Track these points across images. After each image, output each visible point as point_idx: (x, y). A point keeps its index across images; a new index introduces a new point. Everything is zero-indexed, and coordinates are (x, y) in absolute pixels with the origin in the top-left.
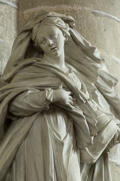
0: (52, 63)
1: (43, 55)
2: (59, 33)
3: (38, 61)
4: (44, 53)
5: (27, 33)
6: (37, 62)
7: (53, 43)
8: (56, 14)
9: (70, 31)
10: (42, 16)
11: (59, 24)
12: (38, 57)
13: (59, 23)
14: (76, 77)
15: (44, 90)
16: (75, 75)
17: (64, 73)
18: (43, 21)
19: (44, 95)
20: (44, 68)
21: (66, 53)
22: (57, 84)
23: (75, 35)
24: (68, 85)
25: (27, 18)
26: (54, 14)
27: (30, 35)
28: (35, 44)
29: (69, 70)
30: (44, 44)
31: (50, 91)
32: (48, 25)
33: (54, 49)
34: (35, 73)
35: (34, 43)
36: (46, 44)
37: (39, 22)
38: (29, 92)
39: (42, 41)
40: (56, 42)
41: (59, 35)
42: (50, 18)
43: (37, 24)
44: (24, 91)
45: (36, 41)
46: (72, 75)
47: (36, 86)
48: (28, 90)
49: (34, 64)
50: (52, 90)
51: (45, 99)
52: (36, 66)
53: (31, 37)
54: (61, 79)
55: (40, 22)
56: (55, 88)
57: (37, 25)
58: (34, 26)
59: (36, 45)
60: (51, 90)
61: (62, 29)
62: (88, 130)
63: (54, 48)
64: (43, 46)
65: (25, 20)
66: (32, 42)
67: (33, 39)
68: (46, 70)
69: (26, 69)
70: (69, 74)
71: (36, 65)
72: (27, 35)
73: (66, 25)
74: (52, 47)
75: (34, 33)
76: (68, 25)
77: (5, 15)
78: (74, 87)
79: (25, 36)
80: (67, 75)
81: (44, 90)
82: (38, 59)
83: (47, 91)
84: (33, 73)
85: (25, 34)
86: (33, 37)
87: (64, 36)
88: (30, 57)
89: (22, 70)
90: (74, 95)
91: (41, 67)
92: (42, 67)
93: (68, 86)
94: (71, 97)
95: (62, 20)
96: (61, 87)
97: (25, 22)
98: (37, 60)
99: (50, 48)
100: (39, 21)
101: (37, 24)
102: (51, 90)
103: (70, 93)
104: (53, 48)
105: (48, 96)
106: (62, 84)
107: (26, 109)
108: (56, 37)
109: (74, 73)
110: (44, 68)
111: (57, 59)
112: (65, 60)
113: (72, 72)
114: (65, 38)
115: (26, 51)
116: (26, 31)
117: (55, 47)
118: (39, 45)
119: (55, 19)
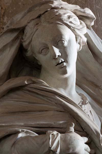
0: (57, 88)
1: (40, 72)
2: (70, 38)
3: (34, 82)
4: (42, 69)
5: (15, 35)
6: (32, 85)
7: (60, 55)
8: (65, 5)
9: (86, 35)
10: (42, 7)
11: (71, 22)
12: (30, 74)
13: (71, 20)
14: (93, 112)
15: (44, 133)
16: (91, 109)
17: (75, 103)
18: (43, 16)
19: (45, 144)
20: (43, 96)
21: (78, 71)
22: (65, 123)
23: (94, 41)
24: (83, 127)
25: (7, 5)
26: (61, 5)
27: (20, 38)
28: (28, 53)
29: (82, 99)
30: (45, 55)
31: (56, 136)
32: (52, 23)
33: (62, 64)
35: (26, 51)
36: (49, 55)
37: (37, 18)
38: (20, 135)
40: (65, 54)
41: (69, 41)
42: (56, 10)
43: (33, 19)
44: (11, 133)
45: (29, 49)
46: (87, 108)
47: (31, 126)
48: (19, 132)
49: (26, 88)
50: (60, 135)
51: (47, 149)
52: (29, 91)
53: (21, 41)
54: (71, 115)
55: (39, 17)
56: (63, 130)
57: (33, 22)
58: (29, 23)
59: (29, 54)
60: (57, 134)
63: (62, 62)
64: (42, 59)
65: (4, 8)
66: (21, 50)
67: (25, 44)
68: (46, 99)
69: (12, 95)
70: (83, 106)
71: (30, 89)
72: (15, 37)
73: (81, 23)
74: (57, 61)
75: (28, 35)
76: (85, 25)
77: (8, 11)
78: (93, 129)
79: (11, 39)
80: (80, 108)
81: (44, 133)
82: (34, 79)
83: (51, 136)
85: (10, 38)
87: (78, 42)
88: (17, 76)
89: (5, 97)
90: (92, 142)
91: (38, 94)
92: (39, 93)
93: (82, 128)
94: (87, 146)
95: (74, 15)
96: (72, 129)
97: (3, 11)
98: (32, 81)
99: (54, 63)
100: (37, 15)
101: (33, 19)
102: (57, 134)
103: (86, 139)
104: (60, 62)
105: (52, 144)
106: (74, 124)
108: (66, 44)
109: (90, 105)
110: (43, 96)
111: (65, 83)
112: (76, 84)
113: (88, 103)
114: (79, 45)
115: (11, 66)
116: (12, 31)
117: (63, 61)
118: (34, 55)
119: (65, 14)
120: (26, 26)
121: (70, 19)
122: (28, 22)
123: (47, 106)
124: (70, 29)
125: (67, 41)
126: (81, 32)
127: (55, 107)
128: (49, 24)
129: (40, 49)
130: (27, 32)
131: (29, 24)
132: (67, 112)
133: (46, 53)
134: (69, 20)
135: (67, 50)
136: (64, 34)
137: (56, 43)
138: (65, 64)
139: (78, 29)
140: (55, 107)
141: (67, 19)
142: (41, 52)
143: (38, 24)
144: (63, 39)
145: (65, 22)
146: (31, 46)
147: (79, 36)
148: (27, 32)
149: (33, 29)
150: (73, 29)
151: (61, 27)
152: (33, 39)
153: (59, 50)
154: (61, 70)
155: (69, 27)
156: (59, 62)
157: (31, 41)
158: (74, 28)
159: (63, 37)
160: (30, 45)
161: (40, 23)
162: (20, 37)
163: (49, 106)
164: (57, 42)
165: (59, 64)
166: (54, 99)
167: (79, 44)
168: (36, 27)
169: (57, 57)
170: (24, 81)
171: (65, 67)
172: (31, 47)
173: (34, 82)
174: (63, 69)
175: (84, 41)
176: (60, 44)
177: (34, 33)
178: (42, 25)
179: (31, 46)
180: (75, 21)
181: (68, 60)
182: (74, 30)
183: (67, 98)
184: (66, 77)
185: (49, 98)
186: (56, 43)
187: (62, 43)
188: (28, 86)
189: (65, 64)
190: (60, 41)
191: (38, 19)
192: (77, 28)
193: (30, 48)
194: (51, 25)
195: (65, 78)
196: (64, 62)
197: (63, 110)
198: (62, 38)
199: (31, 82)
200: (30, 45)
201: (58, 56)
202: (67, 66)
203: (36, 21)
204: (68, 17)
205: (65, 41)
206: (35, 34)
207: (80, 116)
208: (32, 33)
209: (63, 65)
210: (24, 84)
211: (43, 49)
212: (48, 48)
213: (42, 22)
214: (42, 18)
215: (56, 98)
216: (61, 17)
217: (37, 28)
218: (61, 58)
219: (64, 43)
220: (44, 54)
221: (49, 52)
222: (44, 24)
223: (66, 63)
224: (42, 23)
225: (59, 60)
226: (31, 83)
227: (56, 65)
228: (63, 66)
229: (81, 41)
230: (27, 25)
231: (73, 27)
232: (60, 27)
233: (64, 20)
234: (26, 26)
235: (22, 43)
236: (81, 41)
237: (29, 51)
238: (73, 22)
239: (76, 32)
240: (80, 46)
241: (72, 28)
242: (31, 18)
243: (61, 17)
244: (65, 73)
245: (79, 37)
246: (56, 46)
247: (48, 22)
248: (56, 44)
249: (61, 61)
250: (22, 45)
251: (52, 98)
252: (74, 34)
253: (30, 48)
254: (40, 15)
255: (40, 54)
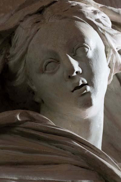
3: (32, 119)
6: (29, 124)
11: (98, 20)
13: (98, 16)
27: (4, 52)
30: (53, 73)
32: (65, 18)
33: (83, 88)
34: (21, 154)
36: (59, 73)
39: (44, 64)
41: (96, 51)
43: (30, 15)
45: (21, 70)
53: (5, 58)
54: (100, 175)
55: (40, 11)
57: (29, 19)
58: (22, 21)
59: (19, 81)
61: (107, 35)
62: (79, 147)
63: (84, 85)
67: (11, 63)
68: (54, 148)
74: (76, 81)
75: (19, 44)
84: (15, 152)
86: (13, 56)
99: (70, 86)
101: (30, 15)
104: (81, 83)
107: (77, 22)
108: (90, 54)
117: (86, 82)
118: (29, 83)
120: (17, 26)
121: (98, 14)
122: (21, 20)
123: (57, 156)
124: (97, 32)
125: (93, 49)
126: (115, 41)
127: (70, 159)
128: (61, 19)
129: (43, 62)
130: (18, 38)
131: (23, 24)
132: (93, 170)
133: (54, 69)
134: (95, 16)
135: (92, 65)
136: (88, 37)
137: (73, 52)
138: (89, 88)
139: (110, 34)
140: (70, 159)
141: (93, 14)
142: (46, 70)
143: (39, 22)
144: (86, 45)
145: (89, 18)
146: (25, 62)
147: (111, 47)
148: (18, 38)
149: (29, 30)
150: (102, 31)
151: (82, 25)
152: (29, 50)
153: (79, 63)
154: (82, 99)
155: (96, 28)
156: (79, 83)
157: (26, 53)
158: (104, 30)
159: (86, 41)
160: (24, 60)
161: (42, 21)
162: (3, 51)
163: (61, 157)
164: (75, 48)
165: (78, 87)
166: (69, 145)
167: (109, 67)
168: (35, 26)
169: (75, 74)
170: (16, 114)
171: (89, 93)
172: (25, 66)
173: (32, 119)
174: (85, 96)
175: (118, 62)
176: (80, 54)
177: (31, 37)
178: (47, 23)
179: (25, 62)
180: (104, 21)
181: (94, 82)
182: (104, 35)
183: (92, 147)
184: (88, 119)
185: (61, 145)
186: (73, 52)
187: (85, 50)
188: (21, 125)
189: (89, 88)
190: (81, 48)
191: (39, 15)
192: (108, 31)
193: (22, 67)
194: (63, 21)
195: (85, 120)
196: (87, 84)
197: (87, 166)
198: (84, 42)
199: (27, 119)
200: (24, 60)
201: (77, 72)
202: (91, 92)
203: (34, 18)
204: (92, 12)
205: (90, 49)
206: (34, 38)
207: (117, 175)
208: (28, 37)
209: (86, 89)
210: (15, 121)
211: (50, 62)
212: (58, 61)
213: (46, 18)
214: (47, 12)
215: (74, 143)
216: (82, 10)
217: (38, 28)
218: (81, 77)
219: (87, 52)
220: (51, 71)
221: (59, 68)
222: (49, 21)
223: (90, 86)
224: (47, 21)
225: (79, 80)
226: (26, 121)
227: (72, 90)
228: (85, 91)
229: (114, 62)
230: (19, 24)
231: (102, 29)
232: (81, 26)
233: (86, 14)
234: (17, 26)
235: (8, 61)
236: (114, 62)
237: (19, 75)
238: (101, 20)
239: (106, 39)
240: (111, 72)
241: (100, 29)
242: (26, 13)
243: (82, 10)
244: (88, 104)
245: (111, 50)
246: (73, 57)
247: (59, 16)
248: (73, 54)
249: (83, 81)
250: (8, 65)
251: (66, 144)
252: (103, 43)
253: (22, 67)
254: (42, 9)
255: (43, 72)
